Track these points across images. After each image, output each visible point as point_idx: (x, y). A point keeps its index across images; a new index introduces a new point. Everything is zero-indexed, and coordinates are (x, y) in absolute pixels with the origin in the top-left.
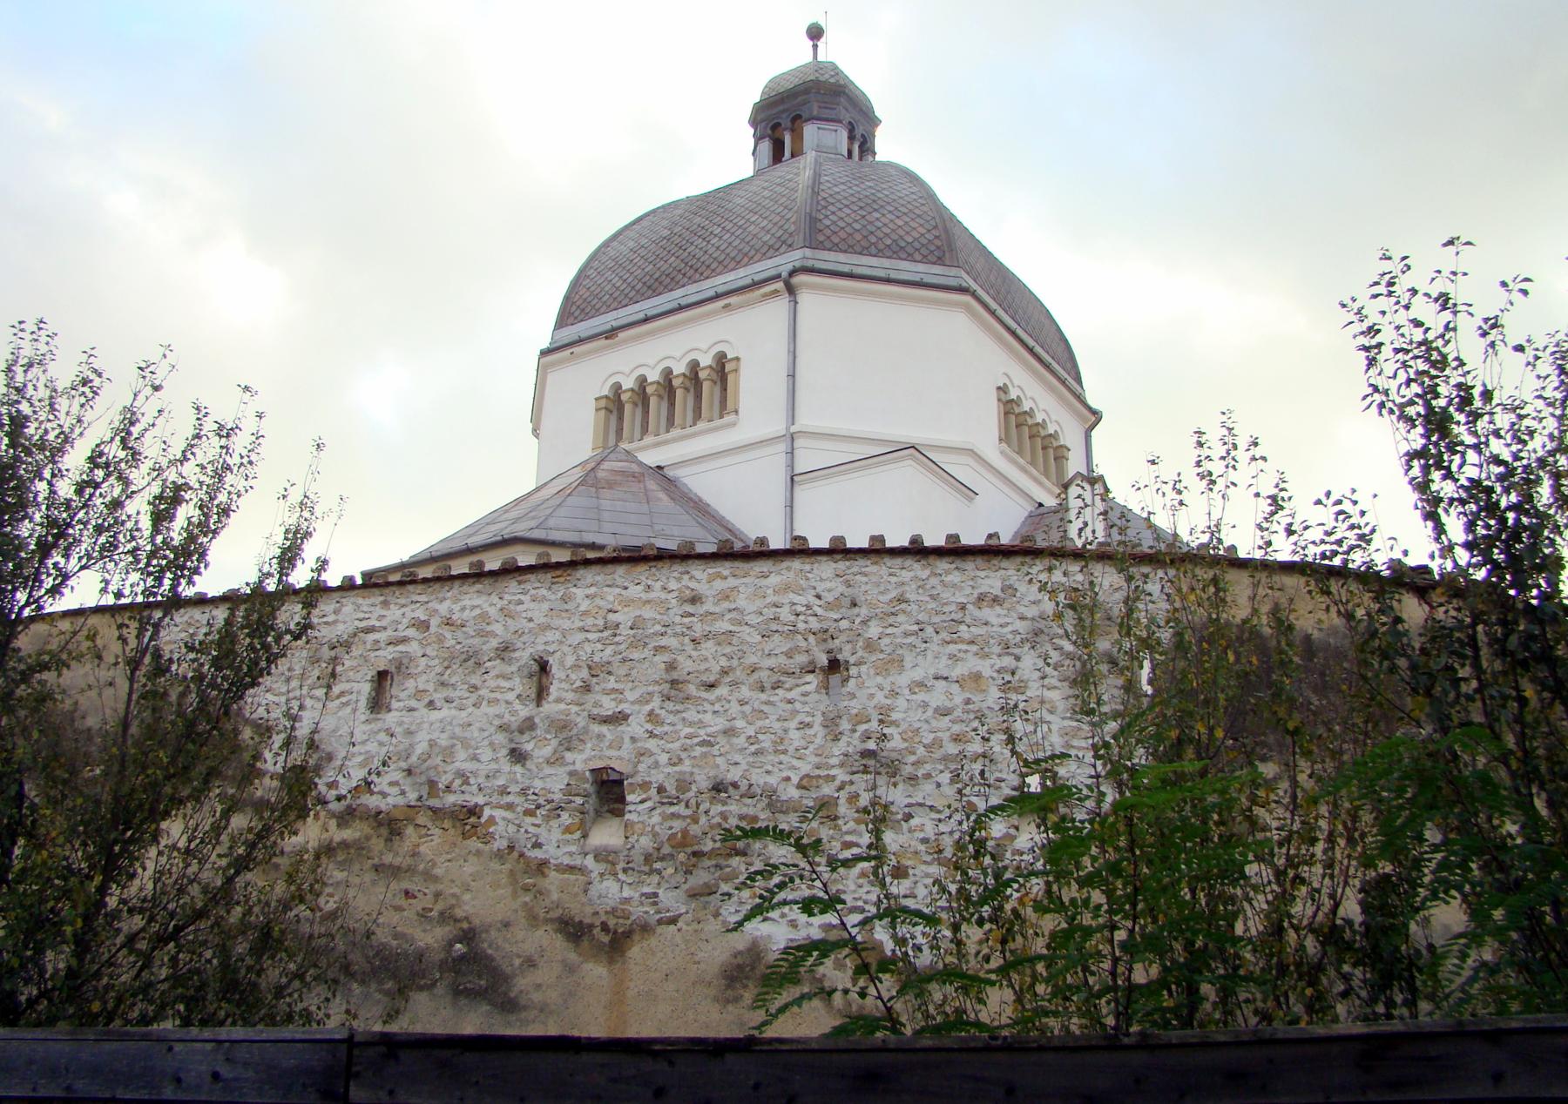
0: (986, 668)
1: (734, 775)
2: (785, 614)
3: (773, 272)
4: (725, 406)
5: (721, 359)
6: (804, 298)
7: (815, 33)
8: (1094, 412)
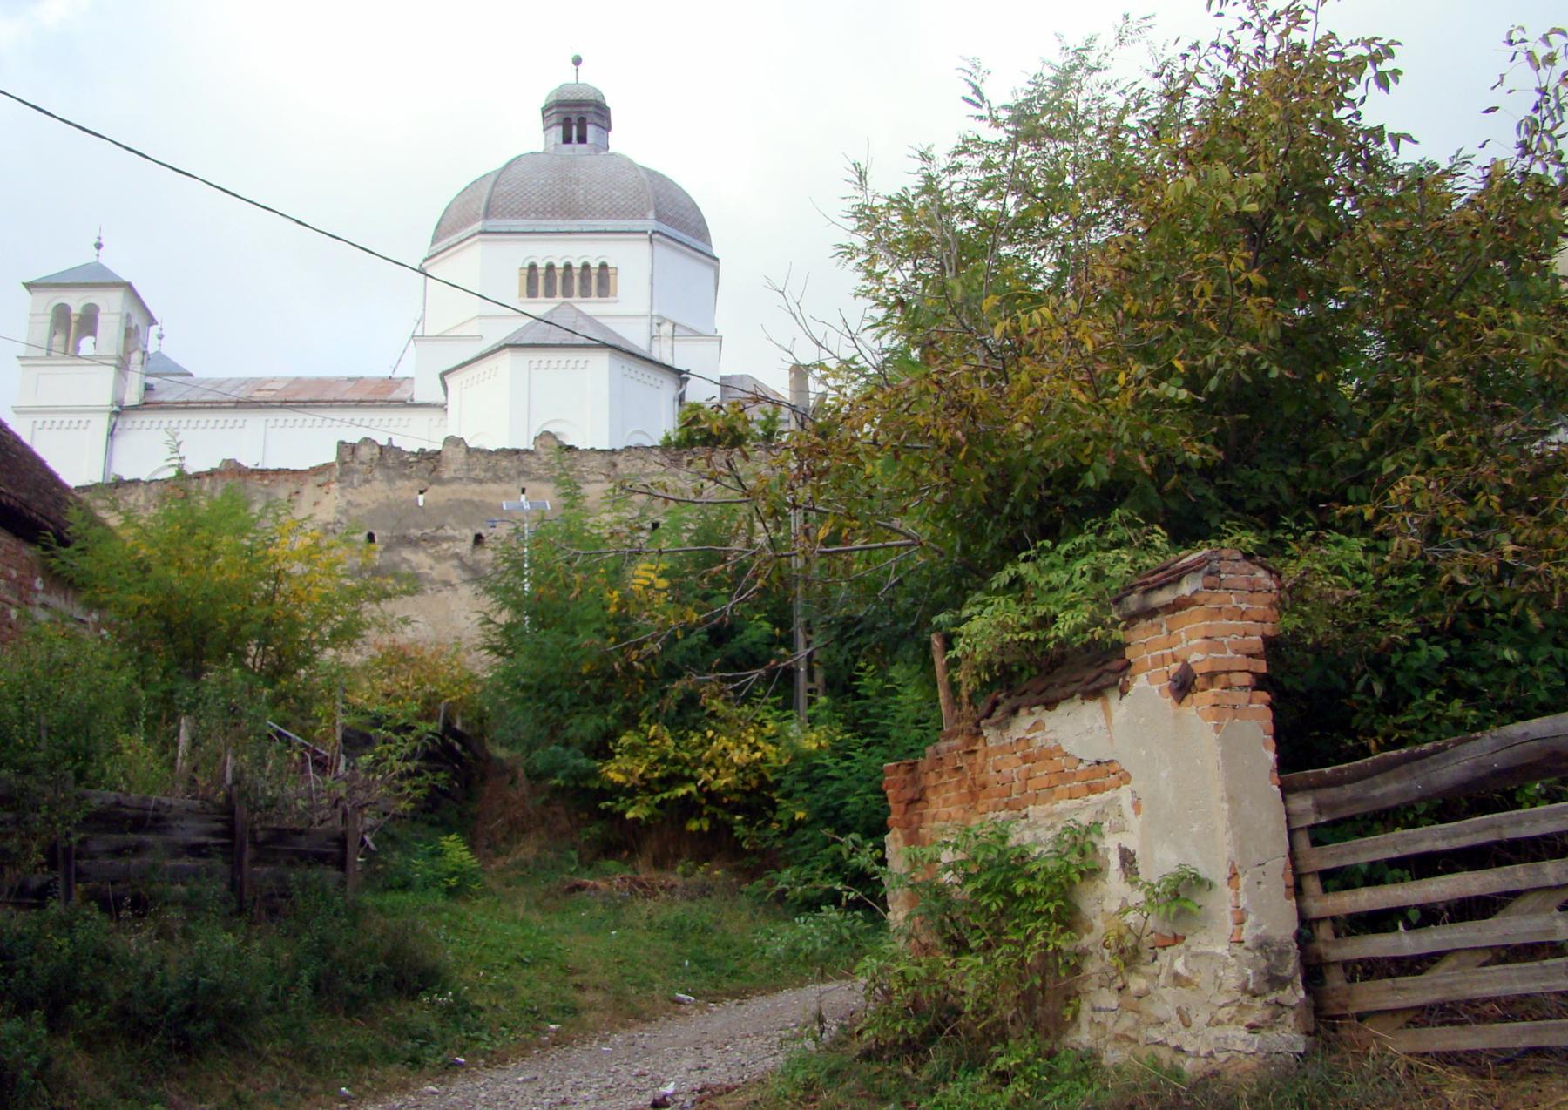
5: (604, 266)
7: (577, 61)
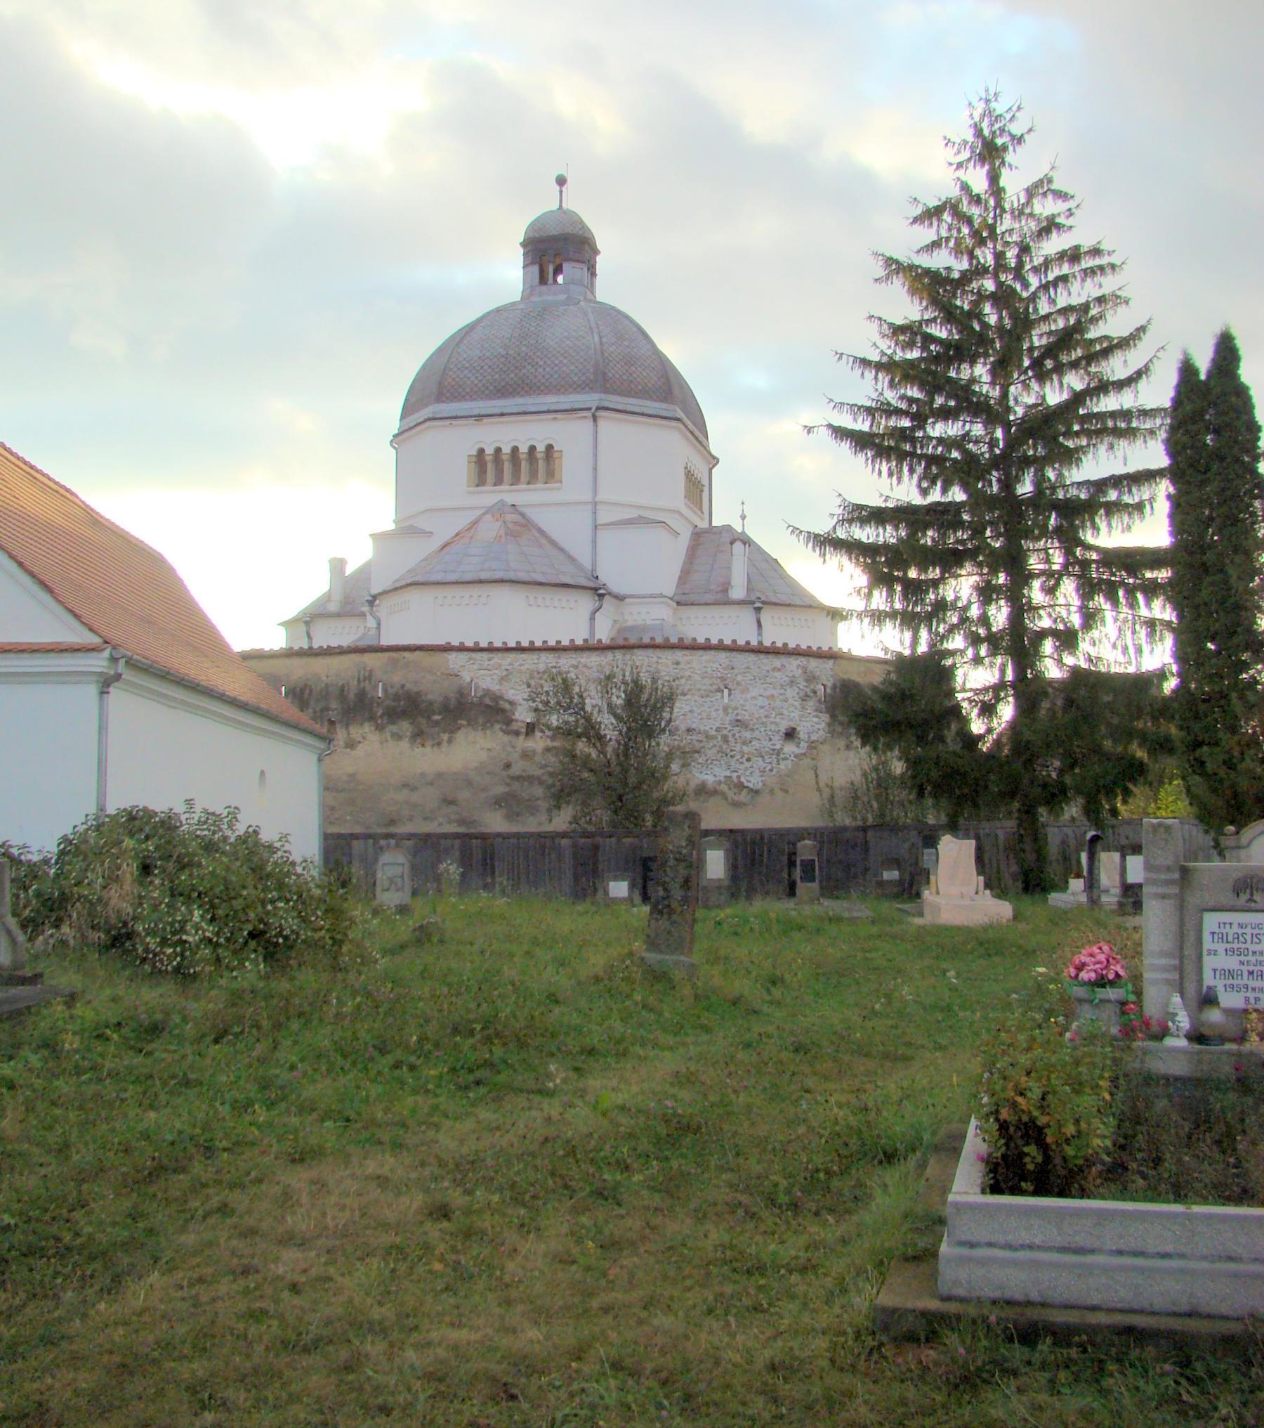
0: (775, 693)
1: (694, 726)
2: (709, 670)
3: (588, 405)
4: (551, 475)
5: (550, 448)
6: (602, 424)
7: (561, 181)
8: (714, 458)
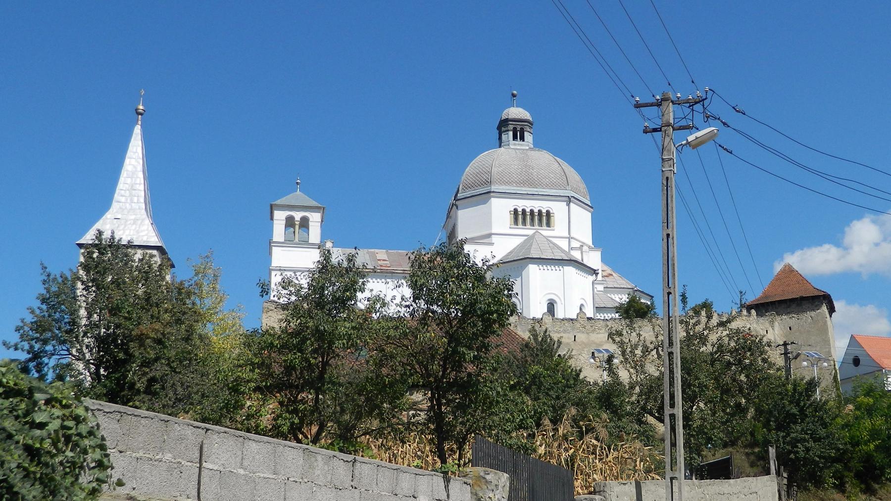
6: (572, 204)
7: (492, 252)
